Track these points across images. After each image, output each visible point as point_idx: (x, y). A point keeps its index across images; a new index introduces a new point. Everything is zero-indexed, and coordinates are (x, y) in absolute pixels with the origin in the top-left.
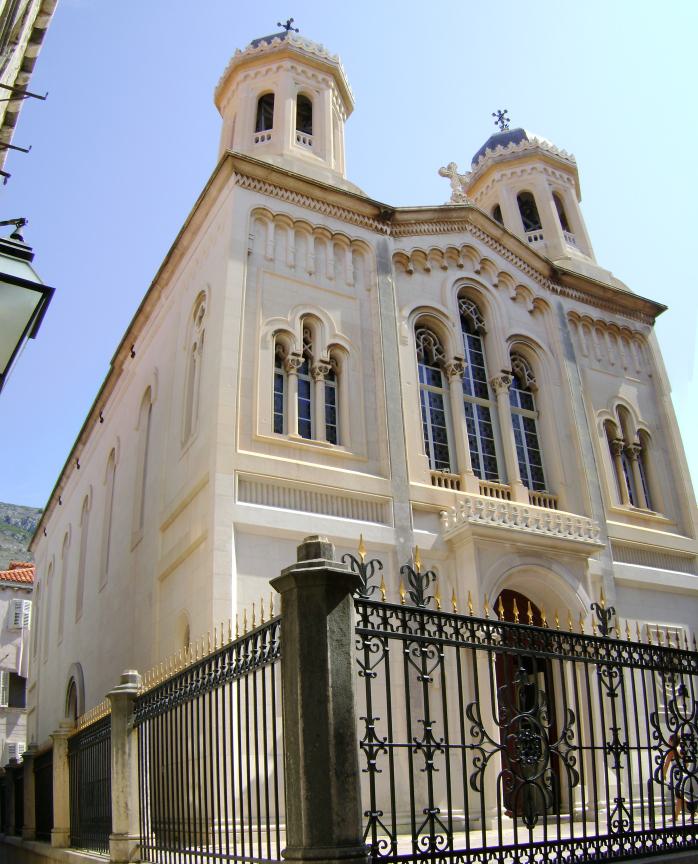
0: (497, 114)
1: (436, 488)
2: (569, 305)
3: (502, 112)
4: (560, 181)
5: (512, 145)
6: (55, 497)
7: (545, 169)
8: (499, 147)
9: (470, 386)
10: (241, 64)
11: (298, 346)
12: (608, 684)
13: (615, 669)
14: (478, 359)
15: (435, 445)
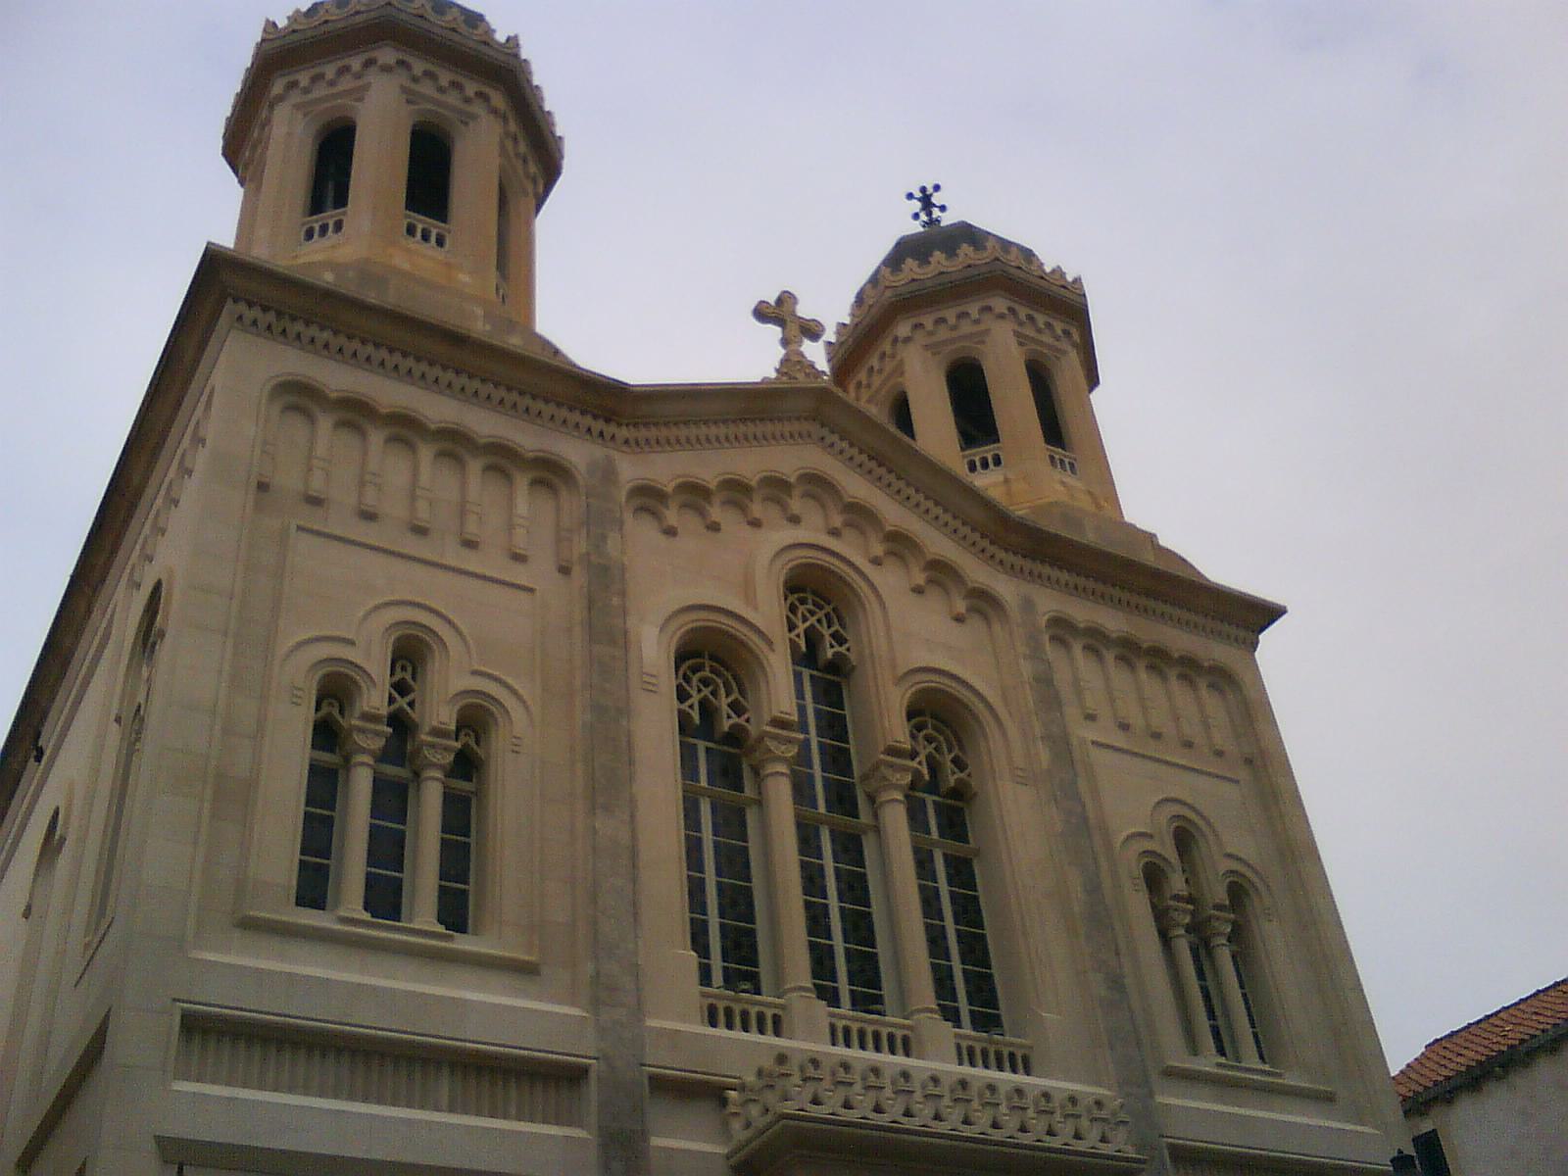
0: (918, 194)
1: (721, 1032)
2: (1049, 602)
3: (930, 190)
4: (1049, 332)
7: (1011, 310)
9: (812, 787)
11: (375, 698)
14: (834, 726)
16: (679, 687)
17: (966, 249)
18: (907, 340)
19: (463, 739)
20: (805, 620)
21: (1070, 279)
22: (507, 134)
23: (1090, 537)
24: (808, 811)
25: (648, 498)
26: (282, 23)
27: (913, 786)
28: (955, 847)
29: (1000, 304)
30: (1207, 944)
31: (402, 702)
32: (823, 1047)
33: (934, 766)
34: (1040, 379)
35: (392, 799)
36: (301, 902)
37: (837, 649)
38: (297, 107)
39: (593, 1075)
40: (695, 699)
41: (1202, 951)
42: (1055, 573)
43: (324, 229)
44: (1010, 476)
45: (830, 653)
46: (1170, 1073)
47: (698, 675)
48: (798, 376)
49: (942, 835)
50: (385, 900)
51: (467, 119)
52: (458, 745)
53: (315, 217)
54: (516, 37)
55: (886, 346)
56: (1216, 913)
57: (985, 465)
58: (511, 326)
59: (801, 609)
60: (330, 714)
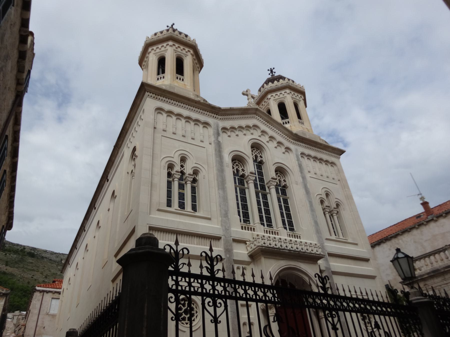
0: (270, 70)
1: (244, 231)
3: (272, 69)
4: (298, 97)
5: (276, 82)
6: (74, 246)
8: (270, 83)
10: (148, 45)
11: (177, 168)
12: (332, 322)
13: (334, 313)
14: (261, 174)
15: (242, 211)
16: (233, 166)
17: (281, 80)
18: (270, 99)
19: (194, 176)
20: (255, 153)
21: (301, 86)
22: (194, 59)
23: (307, 137)
24: (285, 197)
25: (224, 129)
26: (150, 37)
27: (276, 185)
28: (285, 197)
29: (288, 91)
30: (332, 215)
31: (182, 169)
32: (287, 238)
33: (280, 181)
34: (296, 106)
35: (181, 187)
36: (167, 206)
37: (261, 159)
38: (154, 54)
39: (222, 238)
40: (235, 169)
41: (331, 216)
42: (301, 144)
43: (161, 78)
44: (291, 125)
45: (260, 160)
46: (327, 239)
47: (236, 164)
48: (251, 105)
49: (282, 194)
50: (182, 206)
51: (186, 56)
52: (193, 177)
53: (158, 76)
54: (195, 39)
55: (266, 100)
56: (326, 207)
57: (286, 123)
58: (198, 96)
59: (254, 151)
60: (170, 171)
